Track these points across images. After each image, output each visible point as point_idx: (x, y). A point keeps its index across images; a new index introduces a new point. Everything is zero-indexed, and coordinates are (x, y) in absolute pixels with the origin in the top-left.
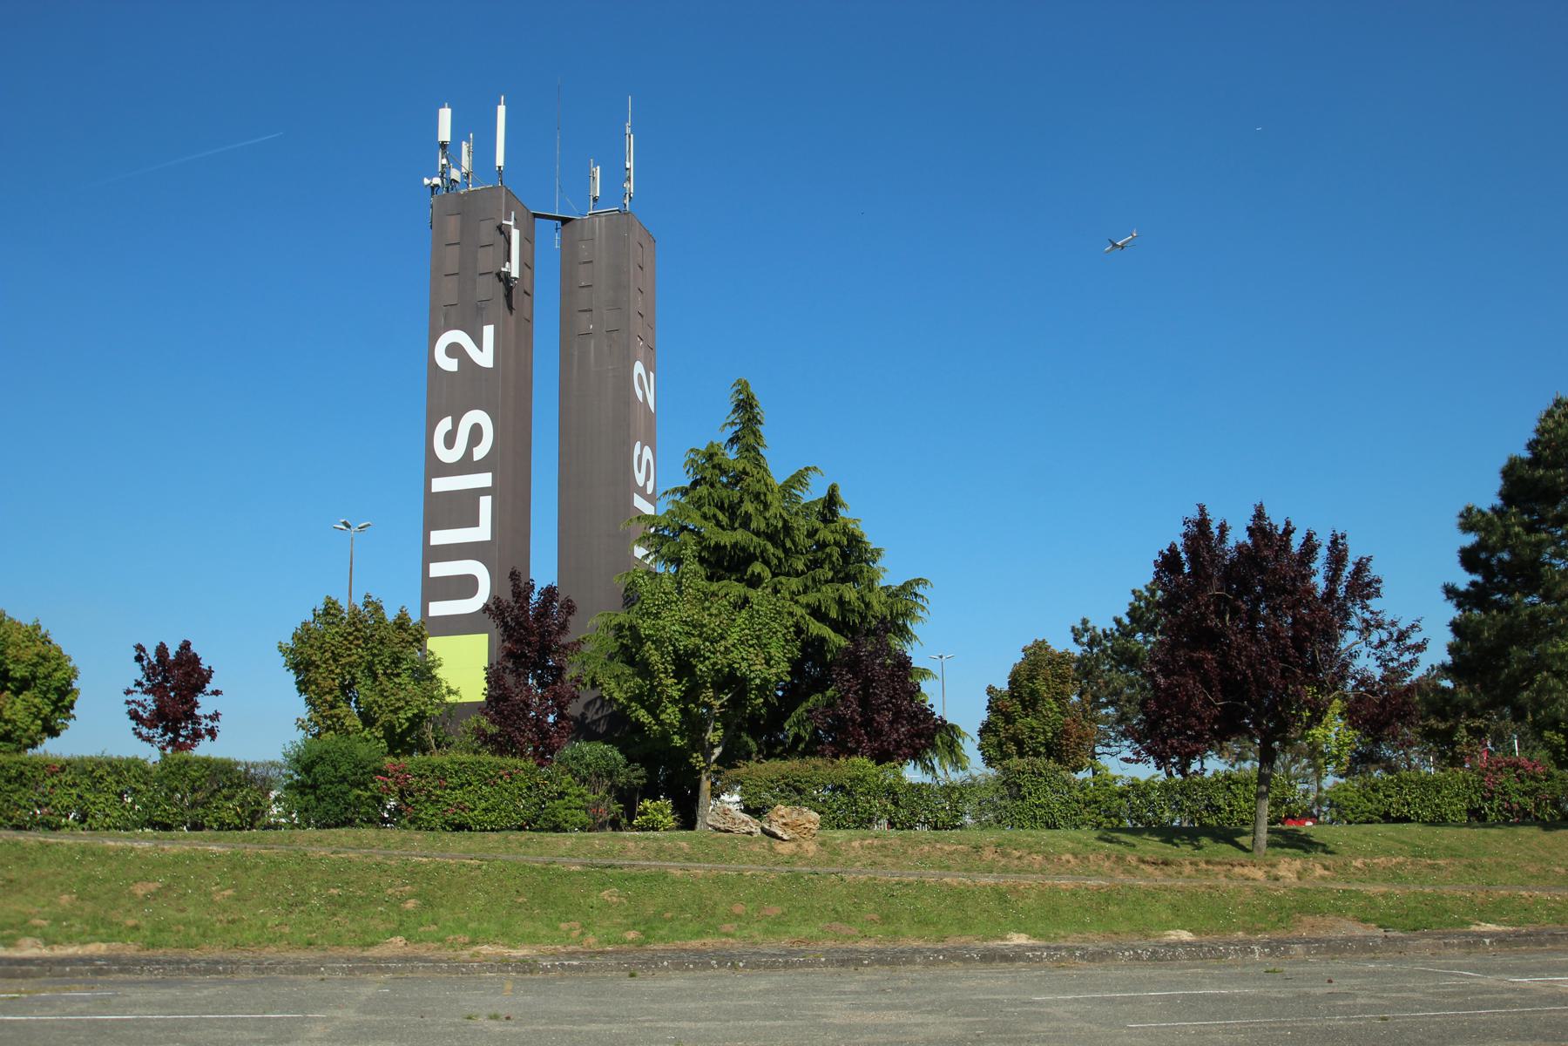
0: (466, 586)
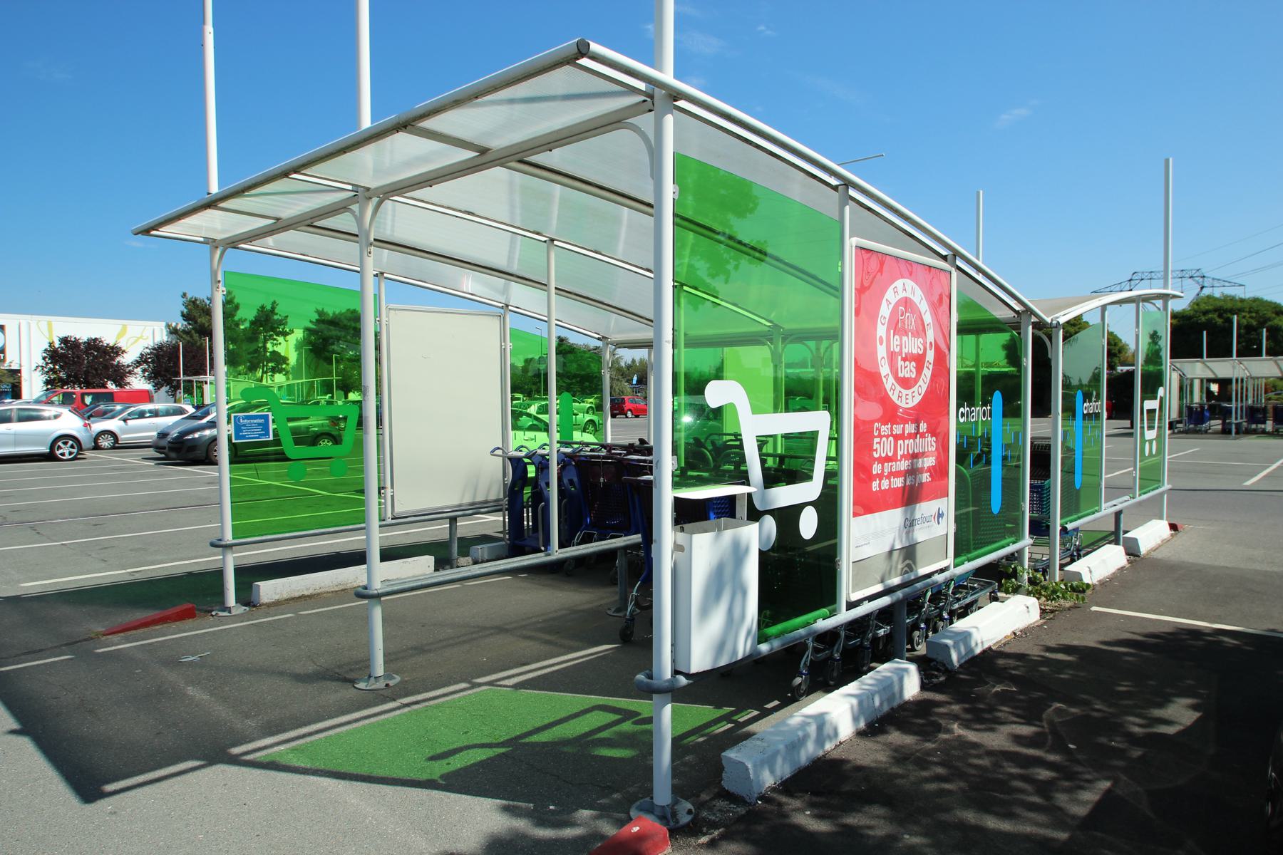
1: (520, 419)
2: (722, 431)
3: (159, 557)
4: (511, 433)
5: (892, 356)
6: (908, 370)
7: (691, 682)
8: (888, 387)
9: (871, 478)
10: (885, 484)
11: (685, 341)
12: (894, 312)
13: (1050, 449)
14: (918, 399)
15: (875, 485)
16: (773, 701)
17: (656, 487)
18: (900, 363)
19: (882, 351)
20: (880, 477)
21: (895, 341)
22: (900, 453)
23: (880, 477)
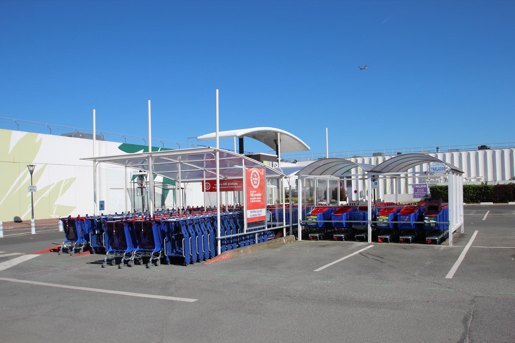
0: (420, 187)
1: (382, 201)
2: (379, 198)
3: (508, 216)
4: (326, 204)
5: (253, 181)
6: (255, 183)
7: (138, 246)
8: (253, 185)
9: (250, 200)
10: (252, 201)
11: (242, 183)
12: (253, 175)
13: (298, 193)
14: (257, 187)
15: (251, 201)
16: (486, 219)
17: (72, 208)
18: (254, 182)
19: (251, 180)
20: (252, 200)
21: (253, 179)
22: (255, 196)
23: (252, 200)
